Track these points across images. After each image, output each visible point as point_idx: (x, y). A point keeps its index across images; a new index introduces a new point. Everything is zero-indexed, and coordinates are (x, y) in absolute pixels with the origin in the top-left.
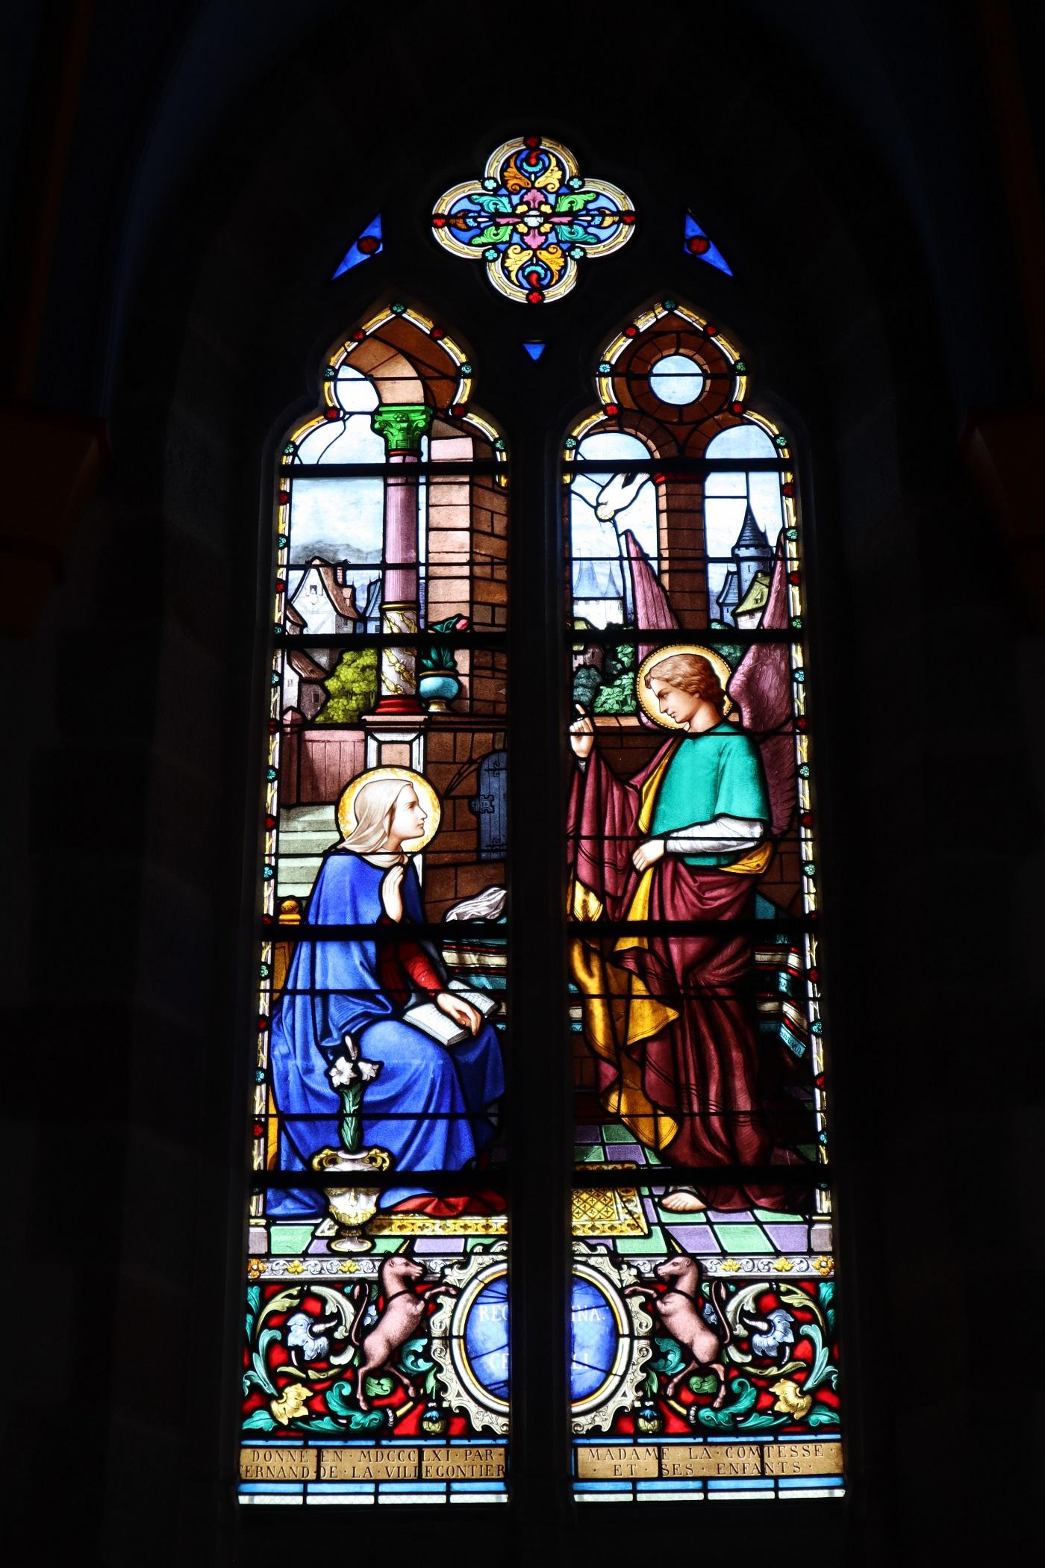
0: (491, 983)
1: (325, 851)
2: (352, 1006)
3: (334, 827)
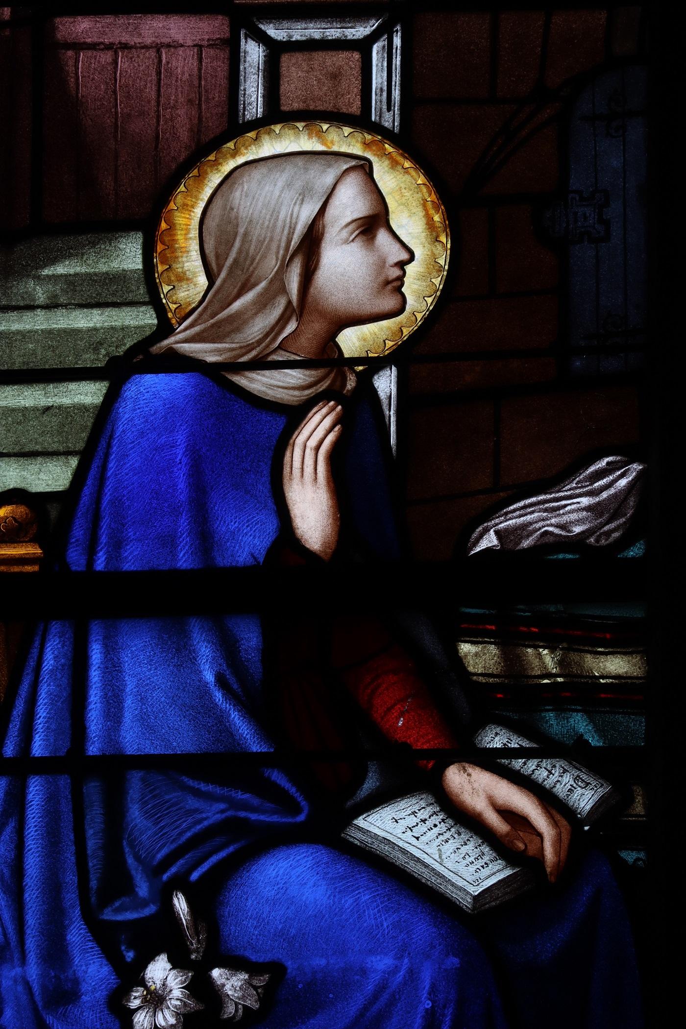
0: (600, 731)
1: (113, 361)
2: (192, 803)
3: (141, 292)
